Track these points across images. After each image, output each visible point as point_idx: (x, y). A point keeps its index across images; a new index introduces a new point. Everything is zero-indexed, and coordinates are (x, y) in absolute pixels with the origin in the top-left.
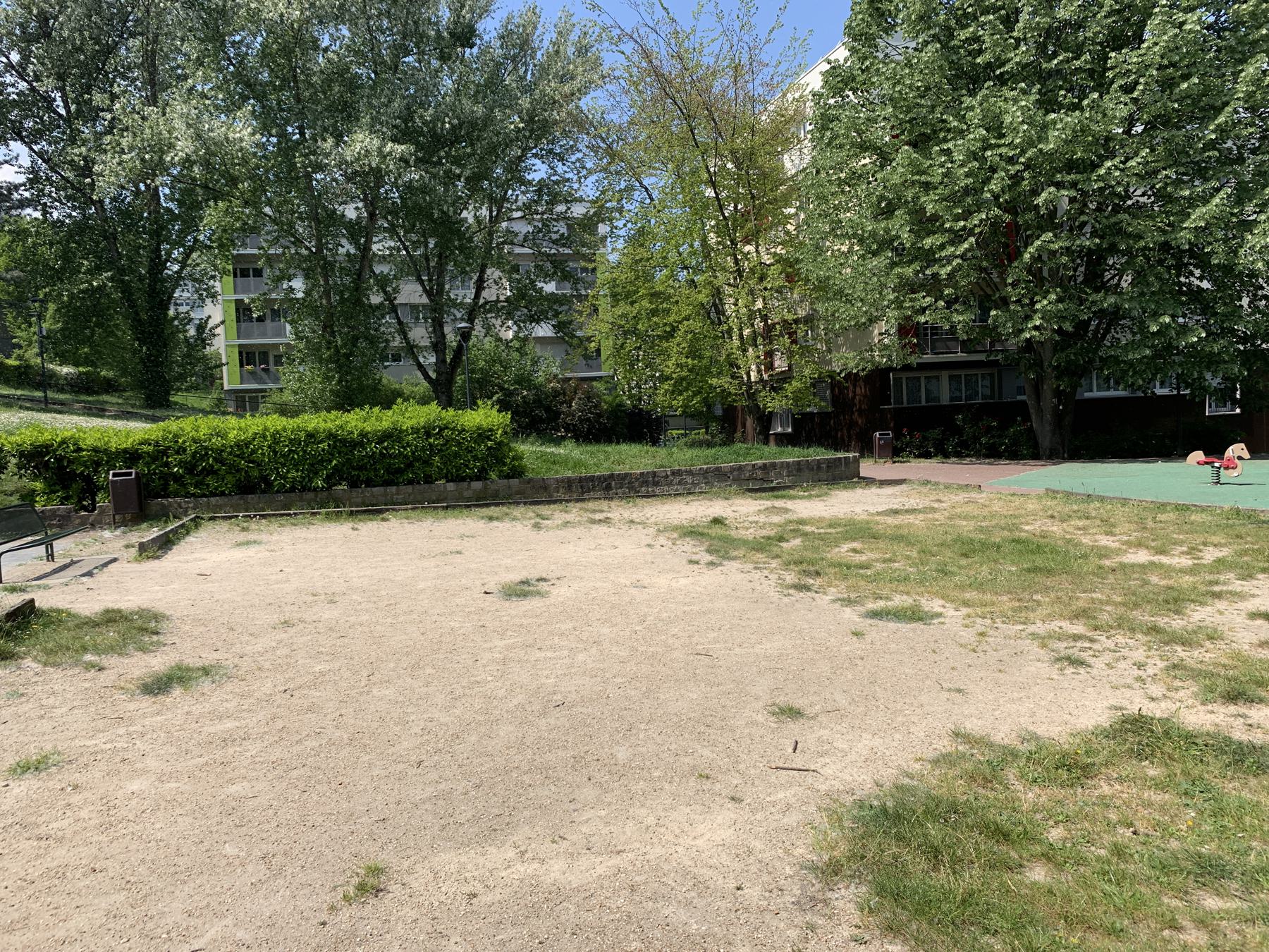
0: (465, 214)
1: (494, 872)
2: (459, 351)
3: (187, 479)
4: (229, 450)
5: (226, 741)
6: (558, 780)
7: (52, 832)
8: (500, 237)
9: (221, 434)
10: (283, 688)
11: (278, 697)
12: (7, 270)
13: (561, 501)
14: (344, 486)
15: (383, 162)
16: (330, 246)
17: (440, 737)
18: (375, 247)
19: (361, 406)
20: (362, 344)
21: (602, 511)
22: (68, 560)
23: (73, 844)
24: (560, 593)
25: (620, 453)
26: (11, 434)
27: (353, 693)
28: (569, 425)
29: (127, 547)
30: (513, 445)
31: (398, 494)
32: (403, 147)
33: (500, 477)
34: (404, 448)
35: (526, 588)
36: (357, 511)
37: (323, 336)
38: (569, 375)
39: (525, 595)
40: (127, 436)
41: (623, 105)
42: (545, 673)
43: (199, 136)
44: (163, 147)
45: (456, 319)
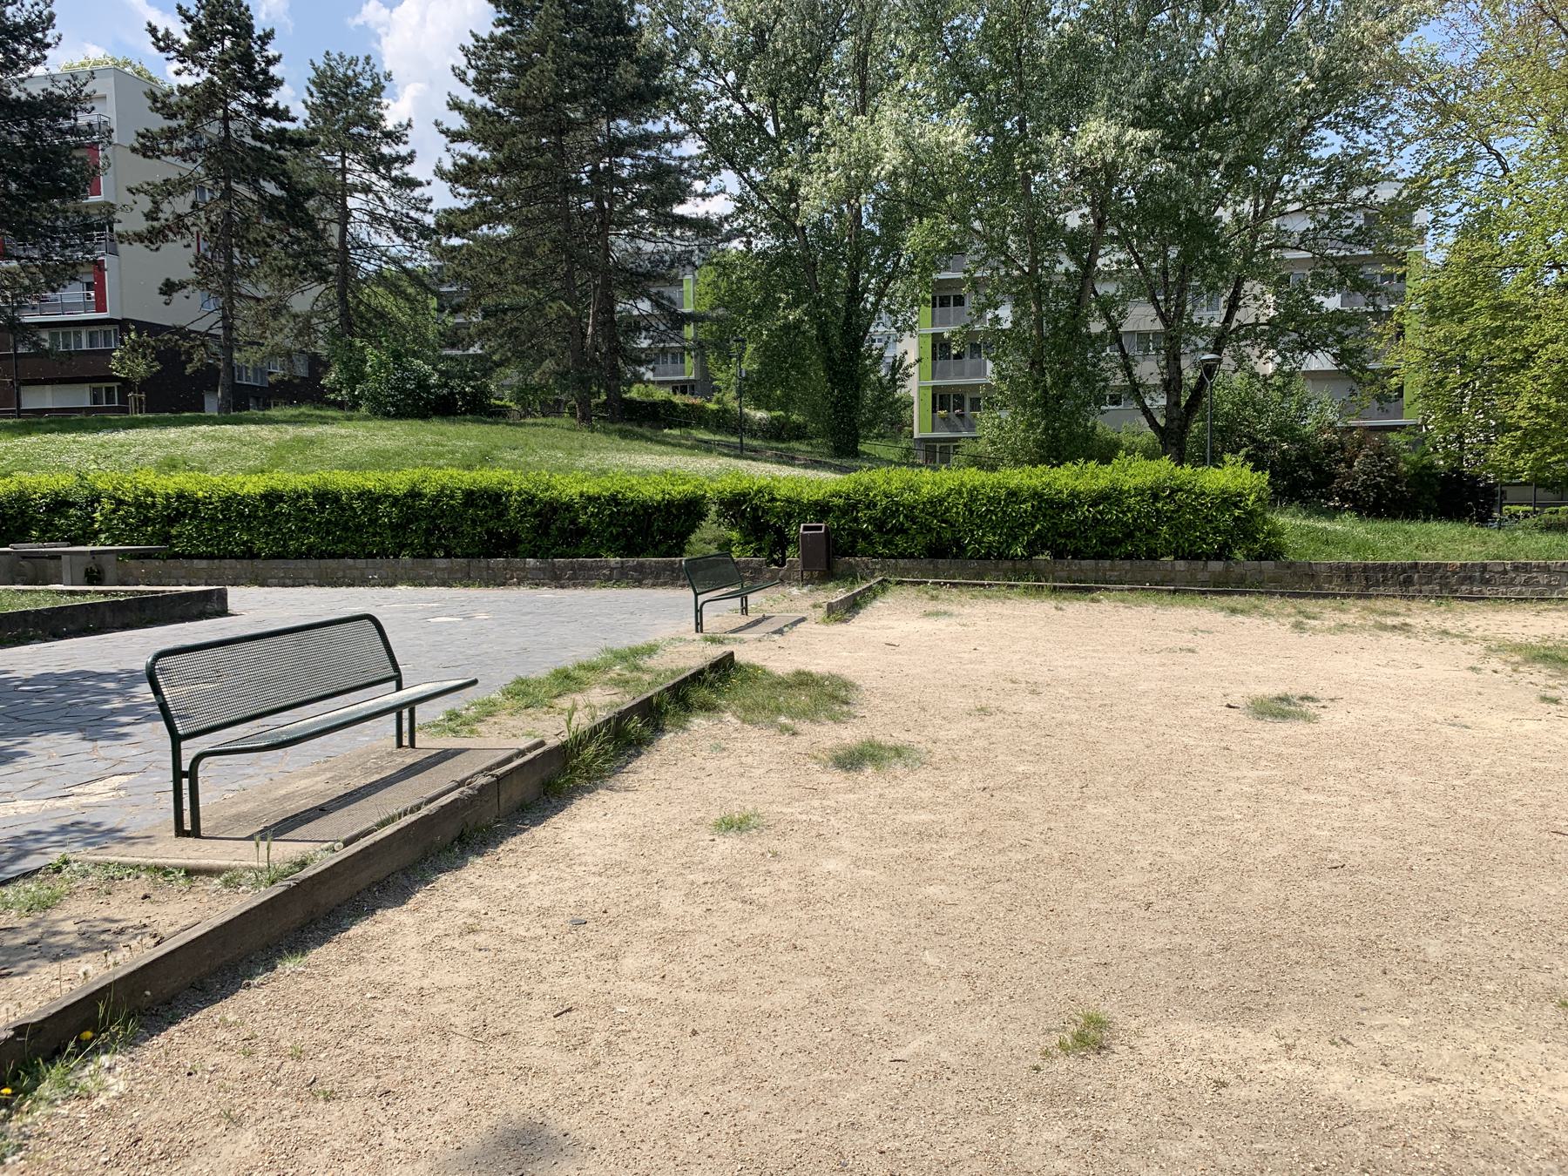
0: (1220, 212)
1: (1250, 1062)
2: (1198, 393)
3: (876, 537)
4: (921, 506)
5: (923, 835)
6: (1338, 963)
7: (755, 897)
8: (1267, 239)
9: (915, 490)
10: (981, 785)
11: (976, 795)
12: (712, 309)
13: (1334, 596)
14: (1045, 556)
15: (1119, 155)
16: (1047, 264)
17: (1173, 877)
18: (1100, 262)
19: (1073, 458)
20: (1075, 383)
21: (1398, 614)
22: (761, 615)
23: (774, 914)
24: (1334, 719)
25: (1428, 534)
26: (712, 480)
27: (1064, 805)
28: (1344, 491)
29: (815, 606)
30: (1268, 515)
31: (1112, 570)
32: (1147, 133)
33: (1247, 557)
34: (1124, 513)
35: (1285, 706)
36: (1061, 588)
37: (1030, 374)
38: (1352, 423)
39: (1284, 716)
40: (819, 488)
41: (1470, 37)
42: (1316, 822)
43: (908, 146)
44: (868, 160)
45: (1198, 349)
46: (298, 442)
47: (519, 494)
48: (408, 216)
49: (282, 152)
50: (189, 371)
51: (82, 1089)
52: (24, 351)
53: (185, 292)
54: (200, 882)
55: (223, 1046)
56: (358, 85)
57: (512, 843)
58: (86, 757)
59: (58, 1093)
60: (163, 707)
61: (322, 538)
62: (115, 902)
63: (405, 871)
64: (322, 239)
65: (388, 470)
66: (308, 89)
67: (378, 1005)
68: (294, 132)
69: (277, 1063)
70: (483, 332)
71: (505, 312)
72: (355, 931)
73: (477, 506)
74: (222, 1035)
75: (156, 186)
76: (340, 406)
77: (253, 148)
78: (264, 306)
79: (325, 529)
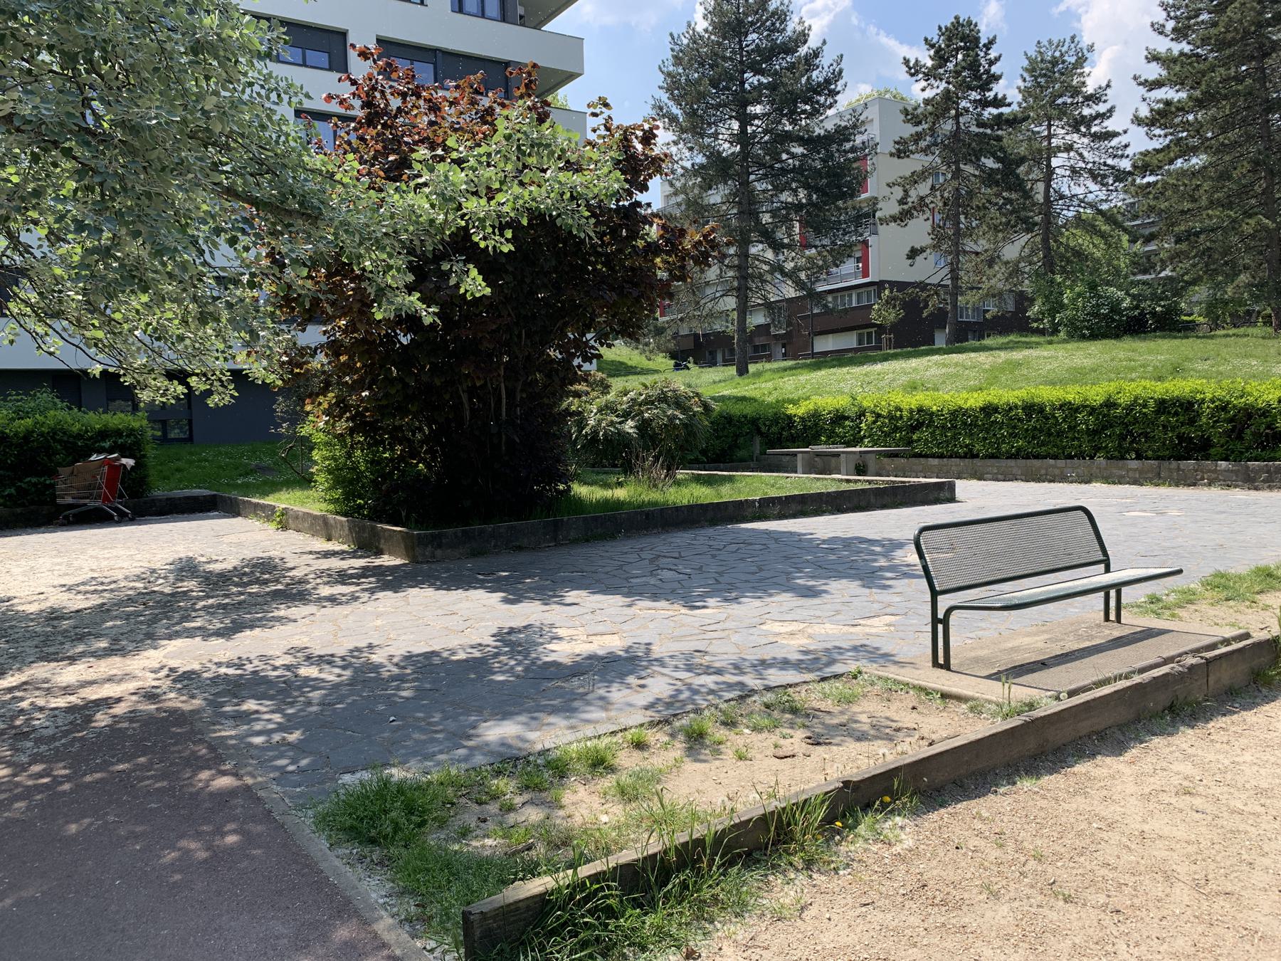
46: (1009, 364)
47: (1212, 401)
48: (1105, 164)
49: (1000, 132)
50: (925, 315)
51: (885, 837)
52: (818, 311)
53: (924, 255)
54: (952, 704)
55: (980, 834)
56: (1064, 62)
57: (1222, 721)
58: (865, 599)
59: (868, 834)
60: (925, 568)
61: (1029, 442)
62: (895, 705)
63: (1122, 727)
64: (1030, 197)
65: (1086, 384)
66: (1022, 76)
67: (1105, 835)
68: (1009, 114)
69: (1023, 859)
70: (1175, 257)
71: (1197, 234)
72: (1080, 768)
73: (1169, 413)
74: (978, 825)
75: (906, 178)
76: (1042, 332)
77: (977, 134)
78: (982, 257)
79: (1032, 434)
